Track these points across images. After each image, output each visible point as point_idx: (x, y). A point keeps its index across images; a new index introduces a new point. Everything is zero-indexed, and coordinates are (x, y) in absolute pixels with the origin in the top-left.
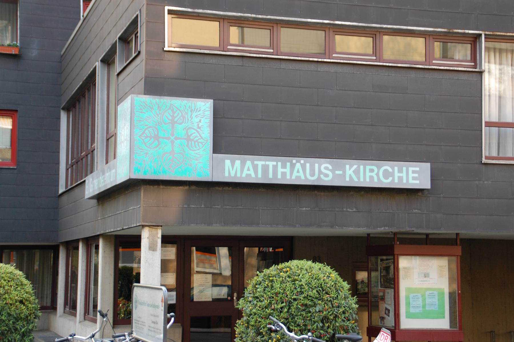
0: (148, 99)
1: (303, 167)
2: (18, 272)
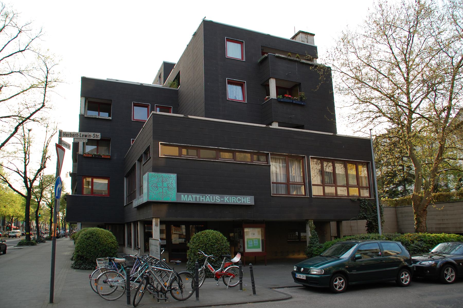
0: (153, 174)
1: (210, 197)
2: (111, 233)
